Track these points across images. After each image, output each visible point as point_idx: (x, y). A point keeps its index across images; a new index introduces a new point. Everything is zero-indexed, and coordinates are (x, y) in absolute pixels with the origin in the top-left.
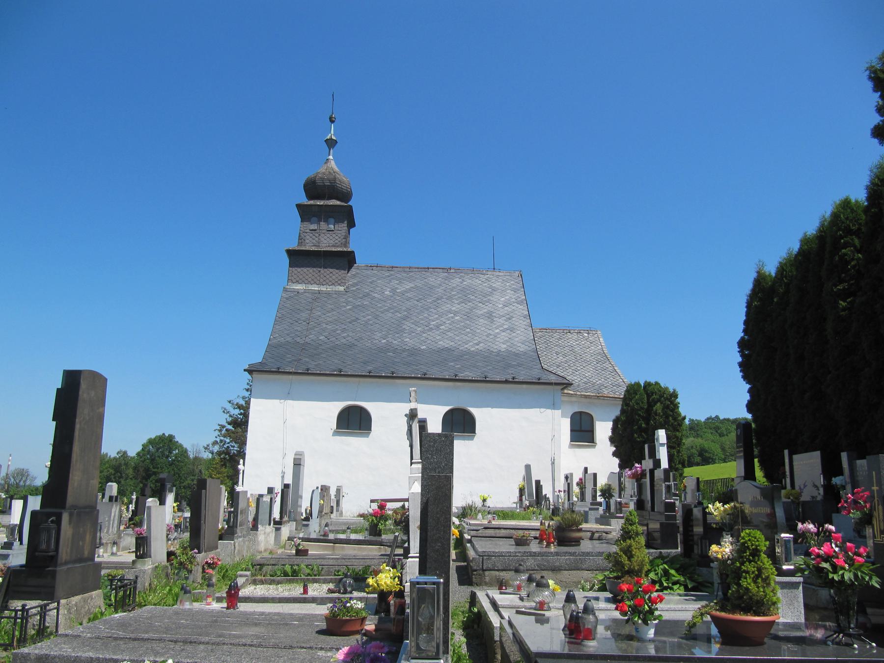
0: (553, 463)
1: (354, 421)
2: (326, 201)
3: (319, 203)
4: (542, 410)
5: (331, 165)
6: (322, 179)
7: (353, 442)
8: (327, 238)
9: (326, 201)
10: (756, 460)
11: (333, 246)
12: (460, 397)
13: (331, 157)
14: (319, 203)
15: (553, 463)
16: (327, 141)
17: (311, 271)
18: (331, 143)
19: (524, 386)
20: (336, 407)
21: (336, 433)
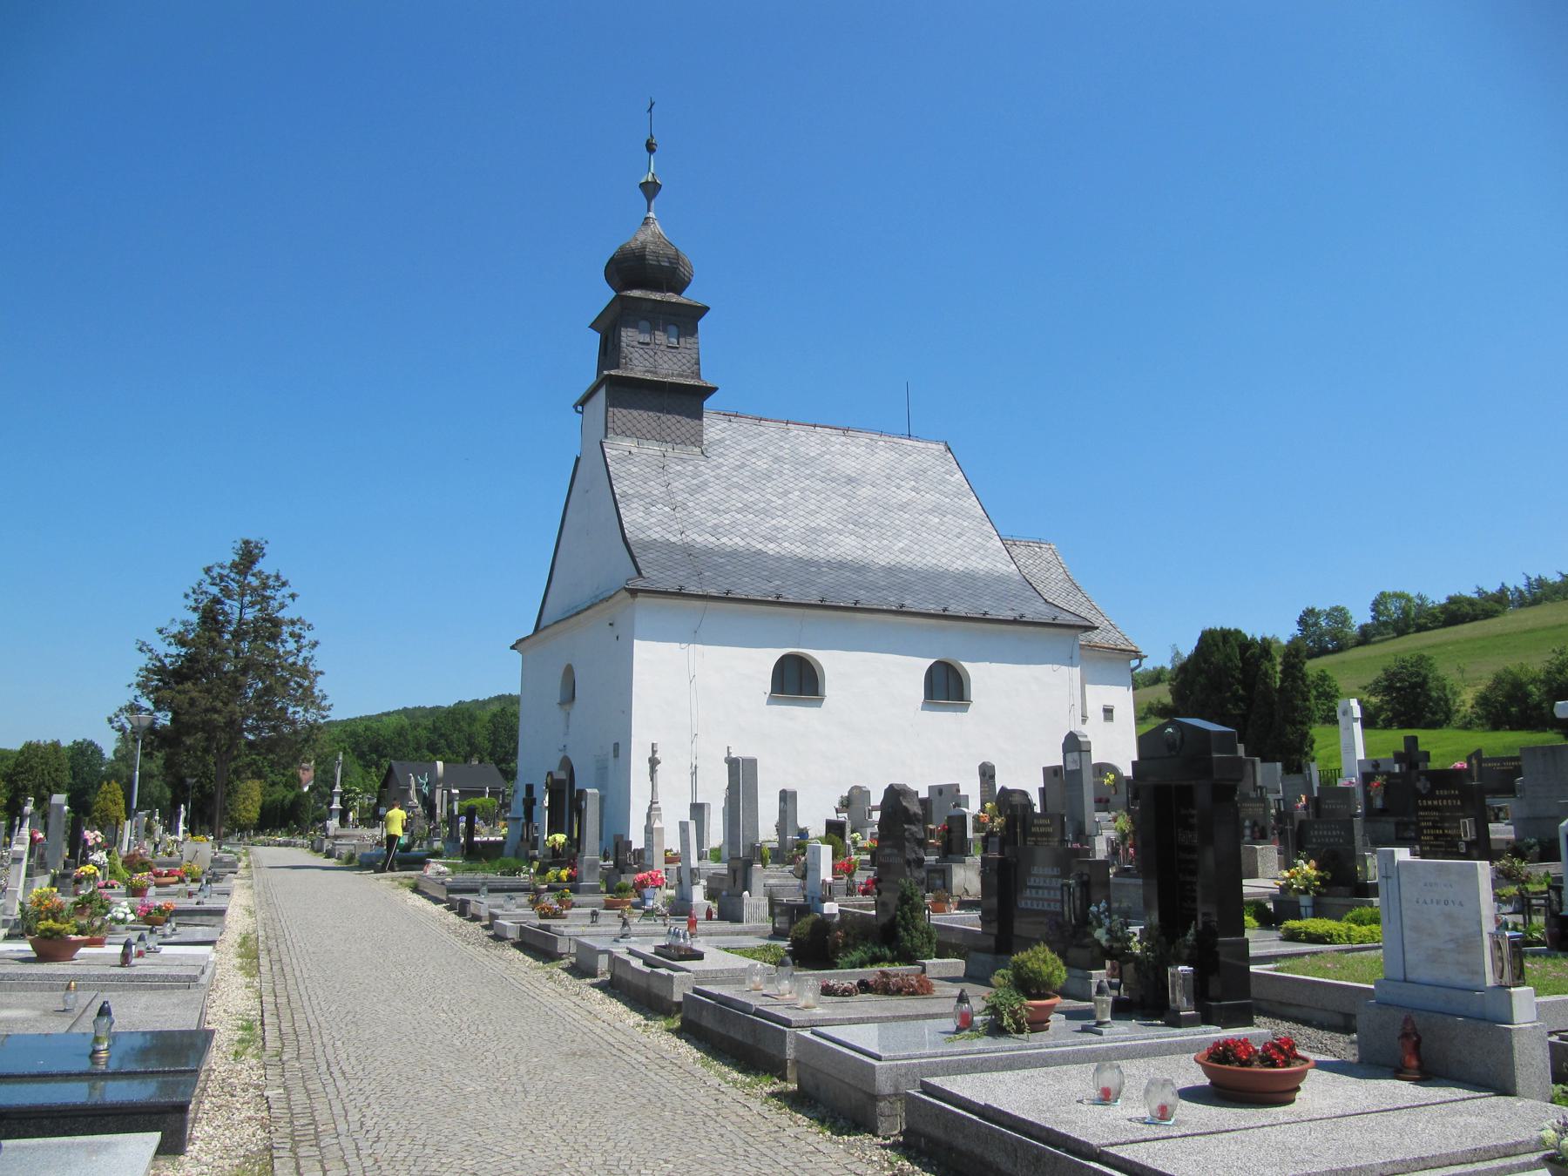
0: (694, 773)
1: (797, 680)
2: (646, 289)
3: (657, 296)
4: (1056, 667)
5: (655, 230)
6: (656, 254)
7: (798, 715)
8: (646, 356)
9: (646, 289)
10: (1037, 809)
11: (680, 375)
12: (949, 644)
13: (652, 214)
14: (657, 296)
15: (694, 773)
16: (641, 185)
17: (645, 415)
18: (650, 190)
19: (1031, 628)
20: (771, 656)
21: (772, 700)
